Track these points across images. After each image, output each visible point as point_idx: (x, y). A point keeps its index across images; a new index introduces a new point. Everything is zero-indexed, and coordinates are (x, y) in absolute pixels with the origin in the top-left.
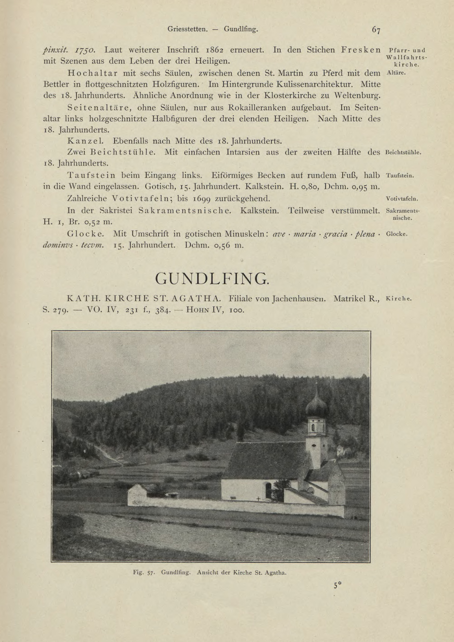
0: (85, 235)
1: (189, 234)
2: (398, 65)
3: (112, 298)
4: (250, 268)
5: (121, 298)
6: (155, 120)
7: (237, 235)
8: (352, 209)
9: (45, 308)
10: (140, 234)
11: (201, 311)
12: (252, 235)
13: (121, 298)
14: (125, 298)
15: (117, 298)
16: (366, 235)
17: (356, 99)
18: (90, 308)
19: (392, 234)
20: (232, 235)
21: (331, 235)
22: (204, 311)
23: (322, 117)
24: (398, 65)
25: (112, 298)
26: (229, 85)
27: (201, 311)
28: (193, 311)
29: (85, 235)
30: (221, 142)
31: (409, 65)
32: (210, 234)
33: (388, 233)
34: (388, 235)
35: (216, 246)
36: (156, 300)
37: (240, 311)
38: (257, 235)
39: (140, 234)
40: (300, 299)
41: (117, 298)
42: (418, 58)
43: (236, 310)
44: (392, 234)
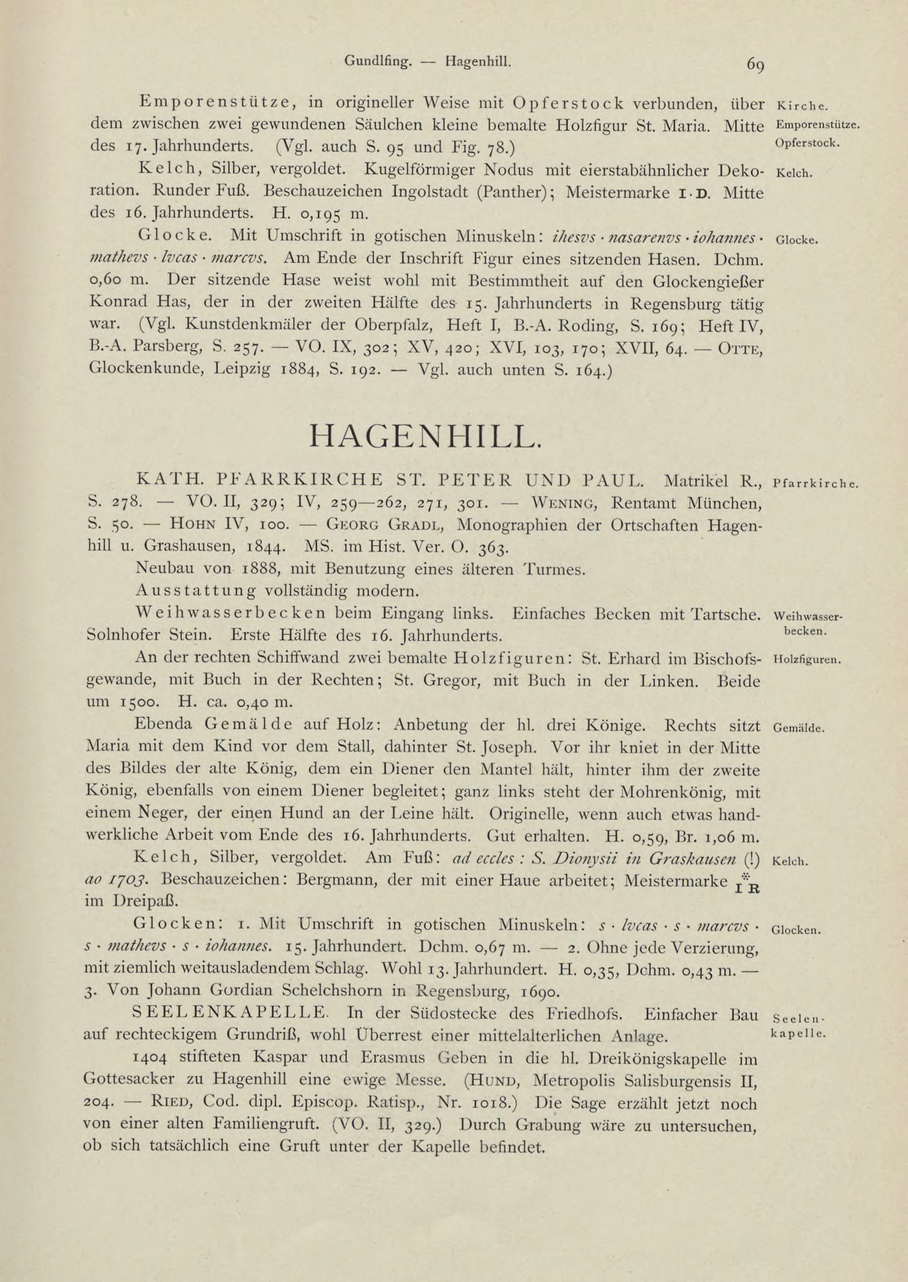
0: (169, 925)
1: (422, 925)
2: (817, 484)
3: (308, 479)
4: (554, 469)
5: (326, 479)
6: (715, 528)
7: (523, 926)
8: (707, 500)
9: (92, 497)
10: (317, 924)
11: (201, 526)
12: (554, 926)
13: (326, 479)
14: (333, 480)
15: (319, 479)
16: (727, 861)
17: (632, 509)
18: (193, 498)
19: (783, 931)
20: (513, 927)
21: (669, 860)
22: (206, 526)
23: (143, 564)
24: (817, 484)
25: (308, 479)
26: (383, 548)
27: (201, 526)
28: (184, 525)
29: (169, 925)
30: (248, 570)
31: (839, 484)
32: (463, 925)
33: (776, 929)
34: (775, 931)
35: (305, 215)
36: (401, 482)
37: (281, 525)
38: (564, 927)
39: (317, 924)
40: (184, 546)
41: (319, 479)
42: (802, 485)
43: (272, 525)
44: (783, 931)
